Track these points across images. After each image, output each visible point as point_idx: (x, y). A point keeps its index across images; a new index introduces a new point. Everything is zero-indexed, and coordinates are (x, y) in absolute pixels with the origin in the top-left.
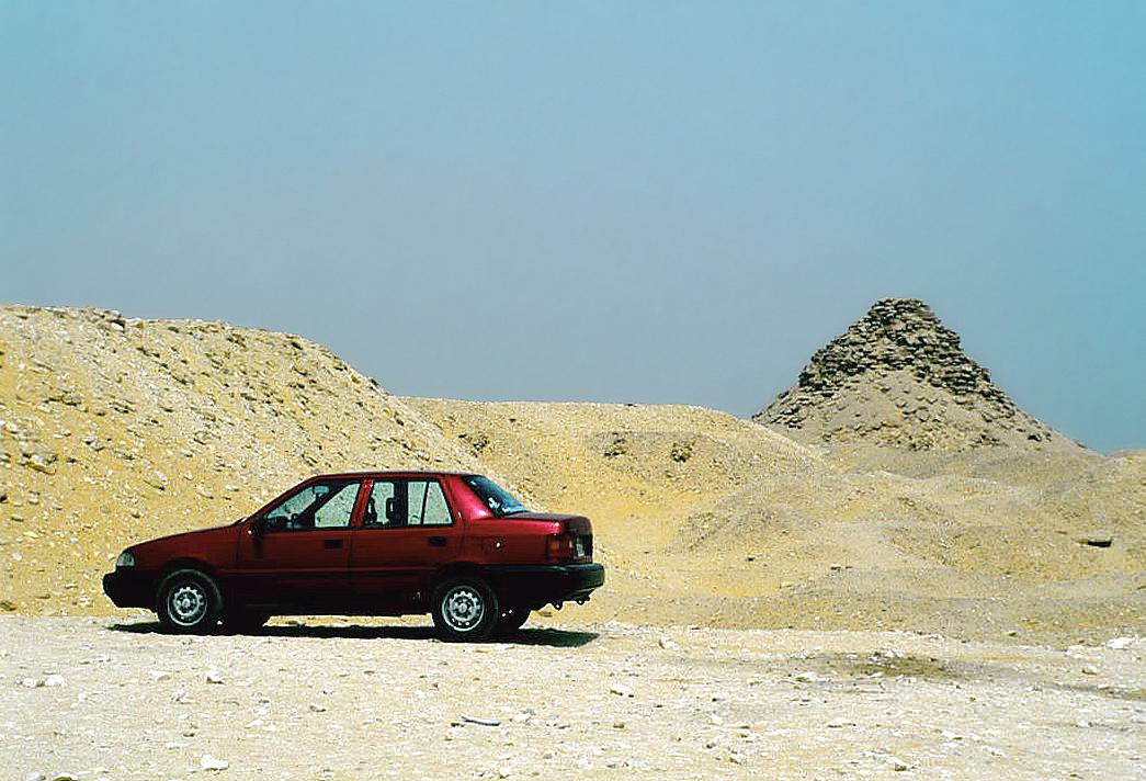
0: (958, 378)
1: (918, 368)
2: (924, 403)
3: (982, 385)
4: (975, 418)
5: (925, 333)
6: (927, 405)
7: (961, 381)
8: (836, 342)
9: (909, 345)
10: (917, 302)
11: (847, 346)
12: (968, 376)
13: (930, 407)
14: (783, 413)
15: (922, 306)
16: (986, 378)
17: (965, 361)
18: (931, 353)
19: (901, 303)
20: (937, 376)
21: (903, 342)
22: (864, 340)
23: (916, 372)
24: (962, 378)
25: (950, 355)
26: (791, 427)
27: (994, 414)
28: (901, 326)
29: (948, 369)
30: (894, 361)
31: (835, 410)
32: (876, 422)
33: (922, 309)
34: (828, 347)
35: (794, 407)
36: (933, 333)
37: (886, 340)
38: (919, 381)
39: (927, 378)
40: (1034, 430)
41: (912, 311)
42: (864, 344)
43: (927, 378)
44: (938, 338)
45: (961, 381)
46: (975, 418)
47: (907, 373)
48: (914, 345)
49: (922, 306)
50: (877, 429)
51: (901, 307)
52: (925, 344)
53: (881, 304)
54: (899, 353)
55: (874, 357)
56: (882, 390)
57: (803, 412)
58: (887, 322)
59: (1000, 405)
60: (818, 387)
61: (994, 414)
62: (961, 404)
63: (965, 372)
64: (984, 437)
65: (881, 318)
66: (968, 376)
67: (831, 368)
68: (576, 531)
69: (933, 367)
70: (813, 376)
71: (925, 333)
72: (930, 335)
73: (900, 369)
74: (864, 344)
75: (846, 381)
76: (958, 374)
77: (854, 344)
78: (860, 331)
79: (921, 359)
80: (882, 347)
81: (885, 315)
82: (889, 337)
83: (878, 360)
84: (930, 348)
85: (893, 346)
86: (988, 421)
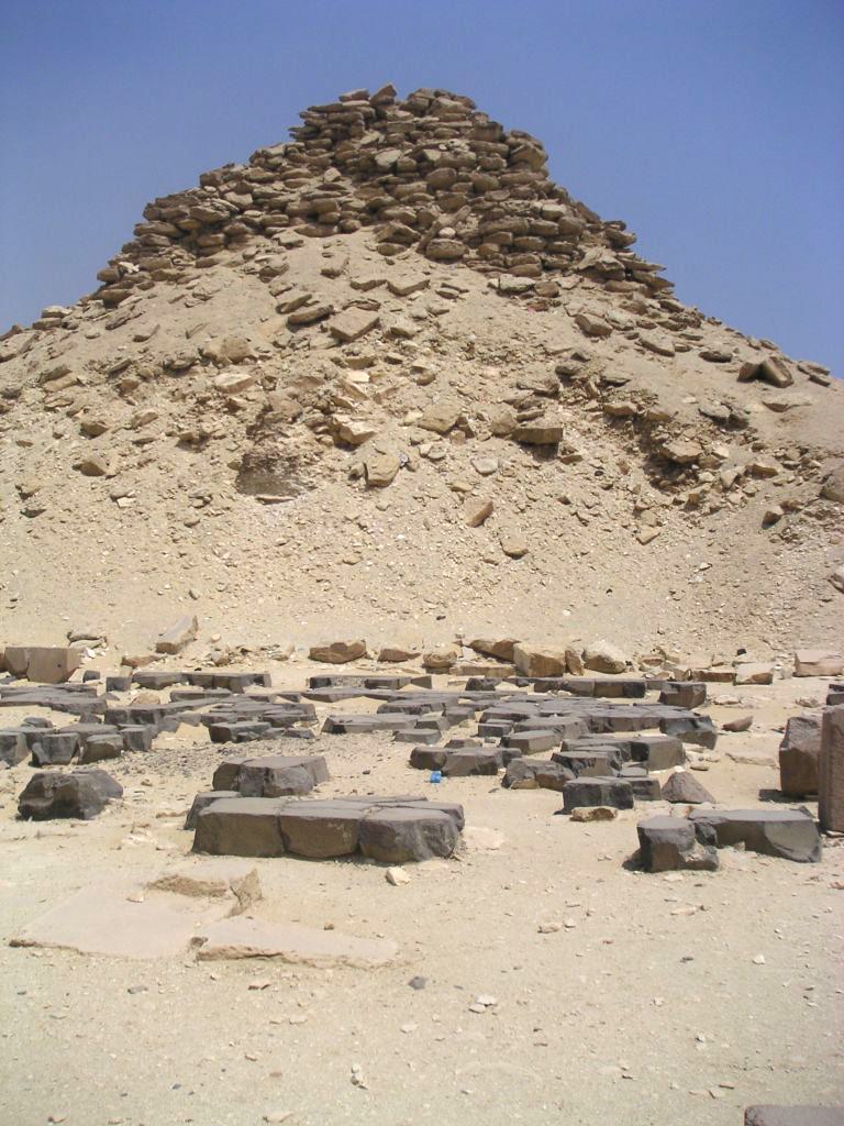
24: (534, 231)
52: (432, 166)
61: (624, 317)
65: (328, 131)
73: (344, 230)
76: (515, 221)
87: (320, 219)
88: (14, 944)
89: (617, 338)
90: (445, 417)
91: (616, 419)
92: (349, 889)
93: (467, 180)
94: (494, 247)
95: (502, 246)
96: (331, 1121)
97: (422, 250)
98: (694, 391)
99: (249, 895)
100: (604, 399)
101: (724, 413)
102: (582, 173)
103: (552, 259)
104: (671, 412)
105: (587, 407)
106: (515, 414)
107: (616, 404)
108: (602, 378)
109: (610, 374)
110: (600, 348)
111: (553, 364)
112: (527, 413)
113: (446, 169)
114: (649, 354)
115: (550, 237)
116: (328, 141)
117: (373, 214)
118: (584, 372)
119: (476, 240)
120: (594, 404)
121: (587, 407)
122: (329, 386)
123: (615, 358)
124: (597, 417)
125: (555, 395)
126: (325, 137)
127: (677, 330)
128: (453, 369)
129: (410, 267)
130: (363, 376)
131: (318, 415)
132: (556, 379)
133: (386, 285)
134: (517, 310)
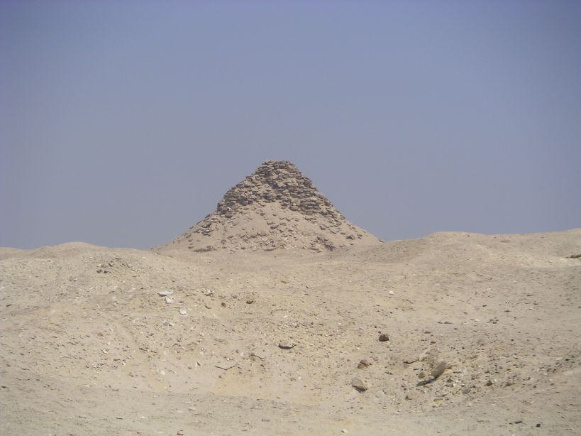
3: (324, 208)
4: (315, 228)
5: (289, 180)
16: (327, 204)
17: (315, 195)
19: (276, 163)
20: (294, 204)
21: (275, 186)
22: (253, 185)
24: (311, 205)
25: (304, 192)
27: (328, 225)
28: (275, 176)
31: (232, 225)
32: (254, 233)
33: (289, 166)
35: (208, 223)
36: (294, 180)
40: (351, 233)
47: (277, 204)
53: (266, 164)
54: (273, 193)
57: (213, 226)
61: (328, 225)
63: (312, 201)
64: (319, 239)
65: (264, 172)
69: (293, 200)
72: (292, 181)
79: (286, 195)
80: (264, 189)
82: (269, 183)
85: (270, 189)
86: (322, 229)
87: (267, 198)
91: (327, 246)
96: (91, 434)
97: (290, 208)
98: (557, 395)
102: (322, 187)
110: (324, 232)
115: (313, 205)
117: (278, 197)
118: (322, 238)
119: (300, 206)
122: (282, 242)
123: (327, 235)
128: (300, 237)
129: (288, 213)
130: (286, 239)
134: (309, 223)
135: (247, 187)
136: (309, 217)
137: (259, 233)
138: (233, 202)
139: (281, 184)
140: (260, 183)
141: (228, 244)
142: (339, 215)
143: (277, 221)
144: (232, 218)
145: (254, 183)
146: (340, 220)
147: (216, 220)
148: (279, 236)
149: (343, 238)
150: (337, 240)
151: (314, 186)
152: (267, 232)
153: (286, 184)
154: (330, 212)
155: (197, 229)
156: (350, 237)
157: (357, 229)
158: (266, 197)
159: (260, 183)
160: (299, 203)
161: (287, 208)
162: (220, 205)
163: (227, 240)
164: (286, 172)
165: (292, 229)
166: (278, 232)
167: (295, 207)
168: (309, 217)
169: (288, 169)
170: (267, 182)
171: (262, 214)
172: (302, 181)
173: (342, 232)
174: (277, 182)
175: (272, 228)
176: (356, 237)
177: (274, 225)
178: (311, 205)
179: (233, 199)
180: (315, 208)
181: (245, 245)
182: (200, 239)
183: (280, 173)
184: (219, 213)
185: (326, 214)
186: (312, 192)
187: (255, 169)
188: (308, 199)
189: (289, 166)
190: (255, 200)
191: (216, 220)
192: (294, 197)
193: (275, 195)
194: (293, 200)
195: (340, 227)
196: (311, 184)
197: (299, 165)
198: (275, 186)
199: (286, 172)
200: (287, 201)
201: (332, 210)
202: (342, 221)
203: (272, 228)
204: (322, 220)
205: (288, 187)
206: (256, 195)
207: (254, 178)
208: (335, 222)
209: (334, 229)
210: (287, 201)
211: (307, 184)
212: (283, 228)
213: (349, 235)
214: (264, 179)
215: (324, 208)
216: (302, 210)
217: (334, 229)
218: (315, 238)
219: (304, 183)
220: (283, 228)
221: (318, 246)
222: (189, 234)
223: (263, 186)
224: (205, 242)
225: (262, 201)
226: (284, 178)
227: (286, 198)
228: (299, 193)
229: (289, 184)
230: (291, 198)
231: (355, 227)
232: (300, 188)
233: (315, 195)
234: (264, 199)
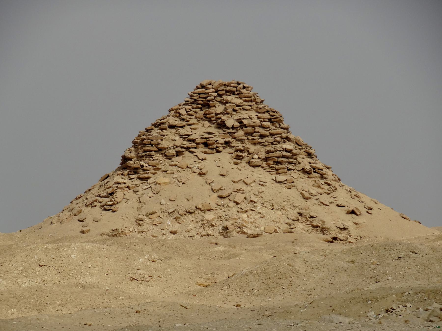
0: (278, 157)
1: (237, 151)
2: (241, 186)
3: (305, 163)
4: (293, 195)
5: (244, 115)
6: (243, 186)
7: (280, 160)
8: (157, 125)
9: (228, 128)
10: (239, 84)
11: (166, 129)
12: (287, 154)
13: (248, 188)
14: (99, 196)
15: (244, 87)
16: (309, 155)
17: (288, 139)
18: (251, 134)
19: (221, 85)
20: (256, 156)
21: (222, 125)
22: (183, 123)
23: (234, 154)
24: (284, 157)
25: (272, 135)
26: (105, 210)
27: (314, 191)
28: (220, 108)
29: (267, 148)
30: (213, 144)
31: (151, 194)
32: (191, 206)
33: (244, 91)
34: (147, 130)
35: (110, 191)
36: (253, 114)
37: (207, 123)
38: (236, 164)
39: (246, 159)
40: (353, 204)
41: (233, 93)
42: (182, 127)
43: (246, 159)
44: (259, 118)
45: (280, 160)
46: (293, 195)
47: (225, 157)
48: (233, 128)
49: (244, 87)
50: (191, 213)
51: (234, 89)
52: (245, 126)
53: (203, 87)
54: (218, 137)
55: (194, 141)
56: (199, 174)
57: (119, 195)
58: (207, 105)
59: (322, 182)
60: (135, 171)
61: (314, 191)
62: (280, 182)
63: (286, 151)
64: (300, 214)
65: (201, 101)
66: (287, 154)
67: (142, 157)
68: (122, 157)
69: (253, 148)
70: (131, 159)
71: (244, 115)
72: (250, 116)
73: (218, 152)
74: (182, 127)
75: (164, 165)
76: (278, 154)
77: (172, 127)
78: (180, 114)
79: (240, 140)
80: (201, 130)
81: (205, 98)
82: (210, 121)
83: (198, 144)
84: (250, 129)
85: (212, 129)
86: (306, 199)
88: (181, 306)
89: (313, 201)
90: (271, 229)
92: (296, 240)
93: (258, 132)
94: (271, 162)
95: (274, 162)
97: (249, 163)
99: (256, 195)
100: (311, 222)
101: (343, 227)
102: (299, 128)
103: (291, 167)
104: (329, 227)
105: (307, 223)
106: (289, 227)
107: (314, 224)
108: (310, 216)
109: (312, 214)
111: (296, 210)
112: (292, 227)
113: (251, 128)
114: (323, 206)
116: (200, 106)
119: (266, 159)
120: (308, 223)
121: (307, 223)
122: (239, 221)
124: (309, 227)
125: (298, 220)
126: (199, 104)
127: (329, 194)
129: (244, 171)
131: (239, 229)
132: (298, 215)
133: (241, 182)
134: (283, 189)
135: (172, 127)
136: (281, 178)
137: (200, 206)
138: (142, 157)
139: (230, 122)
140: (194, 121)
141: (147, 225)
142: (330, 172)
143: (228, 186)
144: (150, 181)
145: (183, 120)
146: (334, 183)
147: (123, 185)
148: (233, 211)
149: (341, 212)
150: (332, 218)
151: (285, 125)
152: (213, 206)
153: (240, 121)
154: (315, 170)
155: (91, 200)
156: (353, 212)
157: (364, 197)
158: (206, 145)
159: (194, 121)
160: (263, 155)
161: (243, 163)
162: (125, 159)
163: (146, 219)
164: (238, 101)
165: (254, 198)
166: (232, 204)
167: (256, 161)
168: (281, 178)
169: (239, 94)
170: (207, 117)
171: (202, 174)
172: (267, 116)
173: (338, 203)
174: (224, 118)
175: (221, 197)
176: (363, 211)
177: (224, 194)
178: (284, 157)
179: (150, 148)
180: (290, 163)
181: (176, 227)
182: (99, 217)
183: (227, 102)
184: (126, 172)
185: (309, 173)
186: (284, 135)
187: (185, 97)
188: (278, 147)
189: (244, 91)
190: (187, 148)
191: (123, 185)
192: (255, 144)
193: (222, 141)
194: (253, 148)
195: (333, 194)
196: (281, 121)
197: (259, 89)
198: (222, 125)
199: (238, 101)
200: (241, 151)
201: (319, 165)
202: (336, 185)
203: (221, 197)
204: (304, 183)
205: (243, 126)
206: (189, 140)
207: (183, 112)
208: (327, 187)
209: (325, 198)
210: (241, 151)
211: (275, 120)
212: (239, 197)
213: (351, 209)
214: (200, 114)
215: (305, 163)
216: (269, 165)
217: (325, 198)
218: (293, 214)
219: (270, 120)
220: (239, 197)
221: (300, 227)
222: (77, 209)
223: (200, 125)
224: (111, 222)
225: (200, 151)
226: (234, 110)
227: (239, 145)
228: (262, 136)
229: (245, 122)
230: (248, 145)
231: (360, 195)
232: (262, 126)
233: (288, 139)
234: (202, 148)
